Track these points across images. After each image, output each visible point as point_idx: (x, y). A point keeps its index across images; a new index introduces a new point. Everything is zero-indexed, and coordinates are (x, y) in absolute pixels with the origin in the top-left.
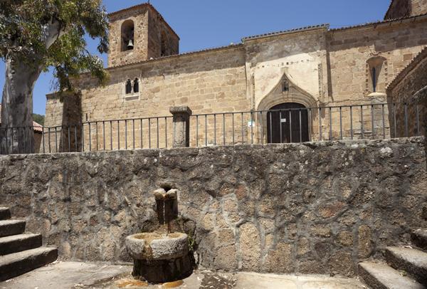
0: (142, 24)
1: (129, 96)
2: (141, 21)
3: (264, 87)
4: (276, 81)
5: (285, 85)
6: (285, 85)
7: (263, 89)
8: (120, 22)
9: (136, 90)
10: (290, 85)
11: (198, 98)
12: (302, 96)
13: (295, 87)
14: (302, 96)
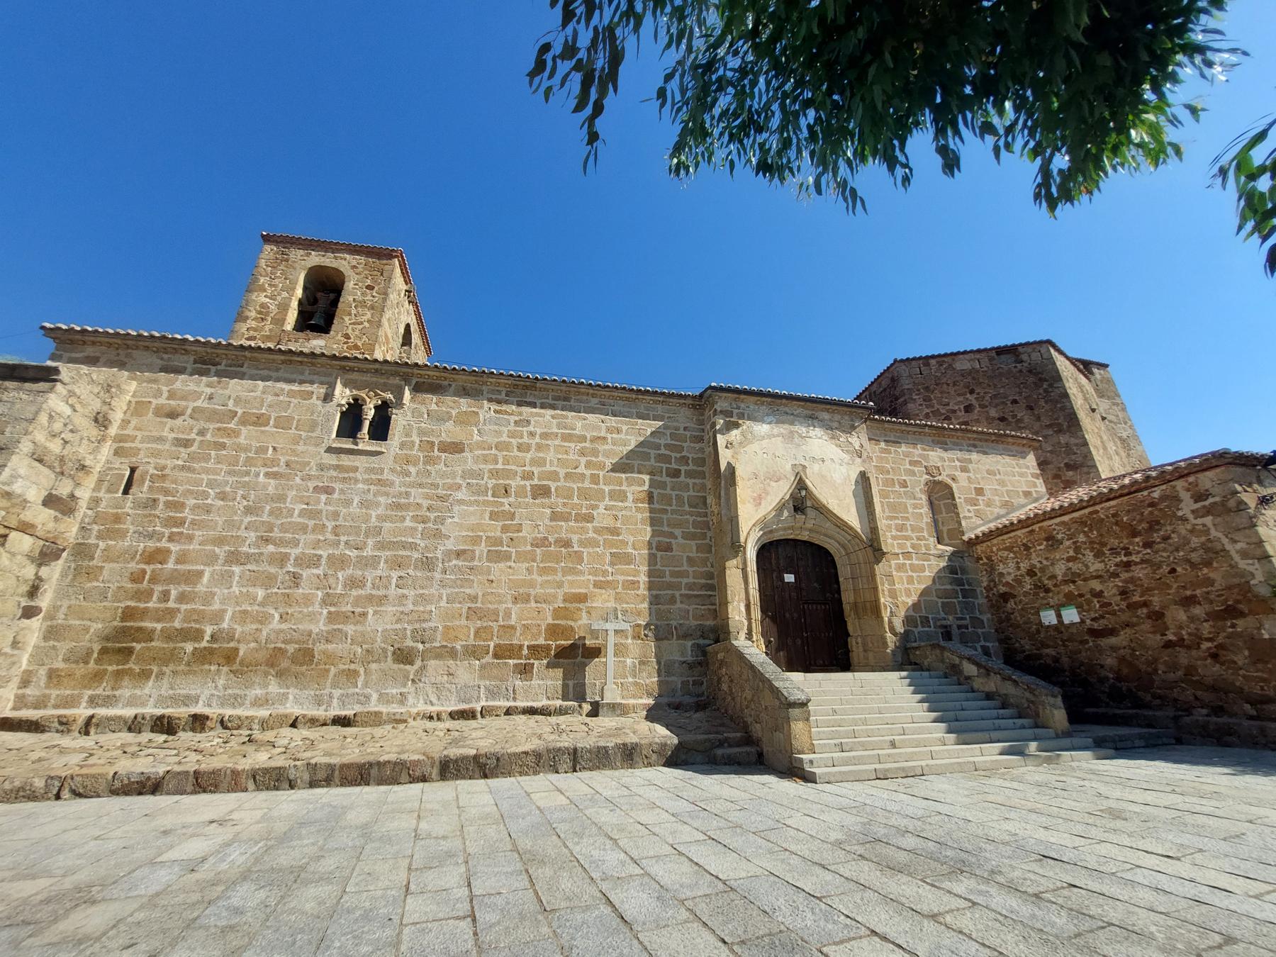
0: (370, 288)
1: (347, 444)
2: (369, 282)
3: (760, 497)
4: (782, 490)
5: (801, 500)
6: (801, 500)
7: (758, 501)
8: (304, 262)
9: (381, 430)
10: (809, 503)
11: (584, 494)
12: (832, 530)
13: (822, 510)
14: (832, 530)
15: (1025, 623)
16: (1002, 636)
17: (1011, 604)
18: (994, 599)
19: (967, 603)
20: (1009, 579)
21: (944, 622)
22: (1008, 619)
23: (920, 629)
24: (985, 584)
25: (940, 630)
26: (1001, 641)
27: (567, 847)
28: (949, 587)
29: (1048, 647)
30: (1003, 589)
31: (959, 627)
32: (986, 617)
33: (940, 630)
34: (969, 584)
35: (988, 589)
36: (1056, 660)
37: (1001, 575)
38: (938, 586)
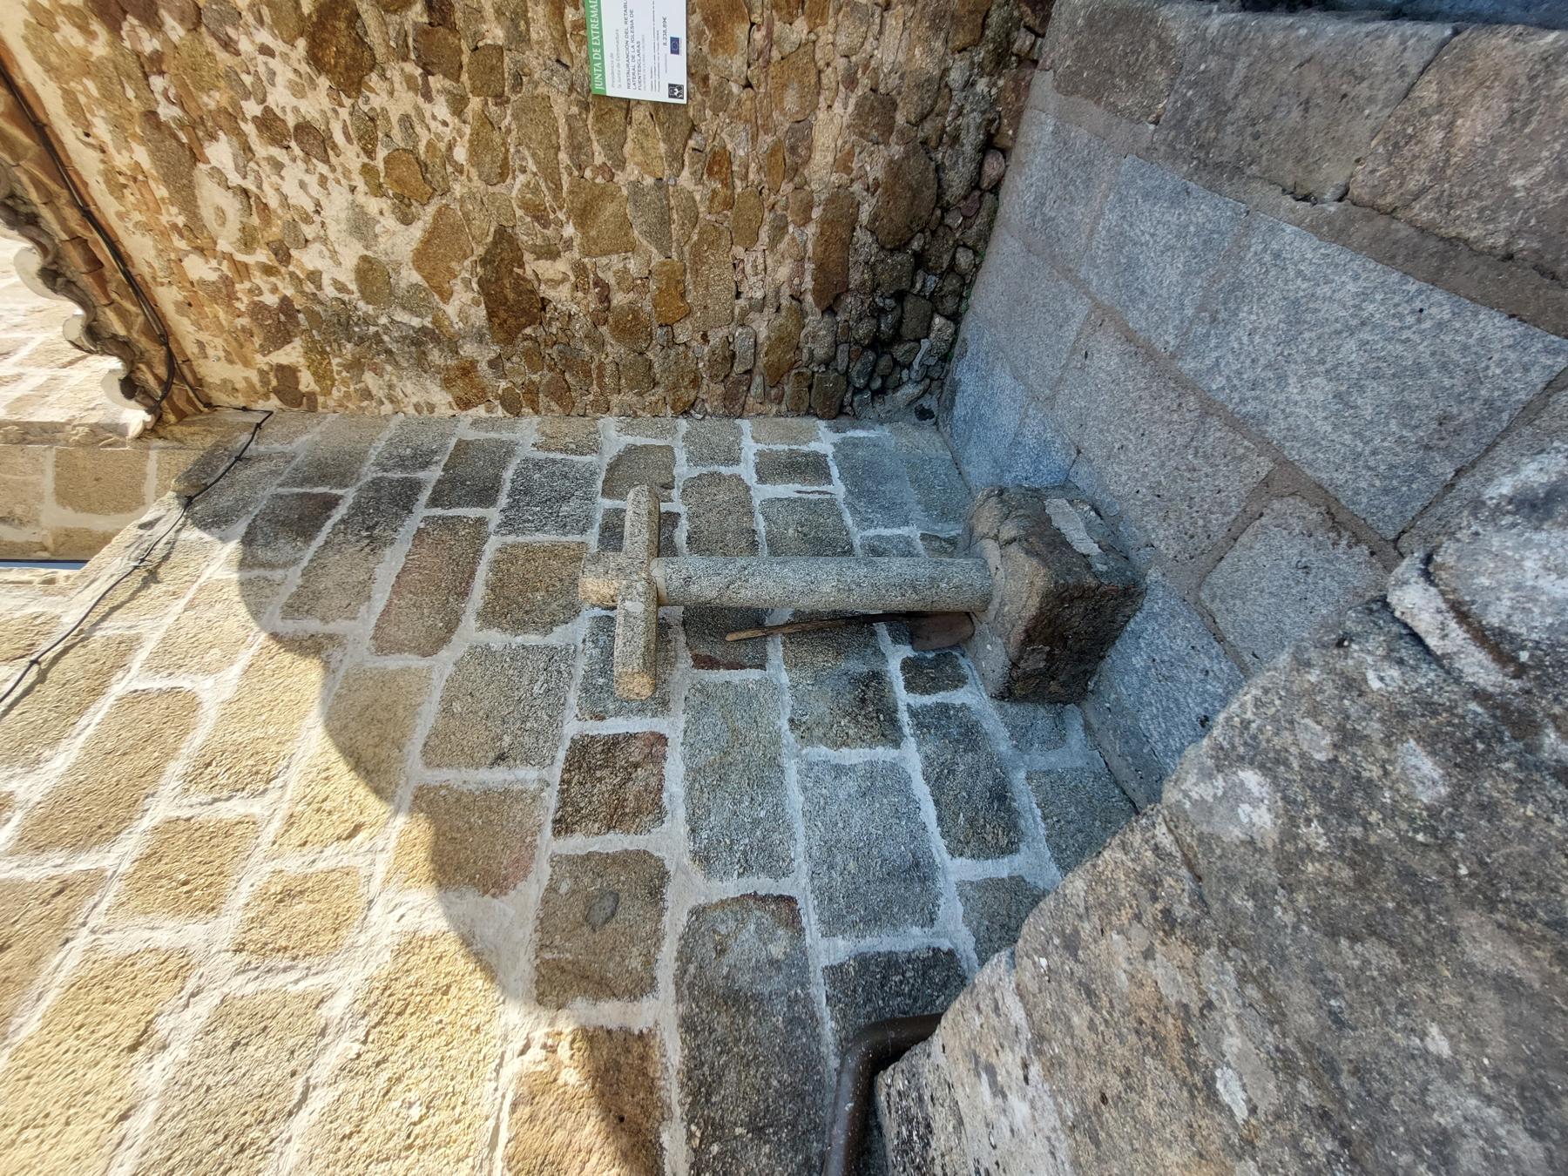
15: (660, 231)
16: (712, 391)
17: (550, 276)
18: (520, 373)
19: (523, 491)
20: (400, 241)
21: (630, 643)
22: (631, 328)
23: (669, 840)
24: (441, 399)
25: (684, 674)
26: (733, 406)
27: (839, 1081)
28: (391, 562)
29: (802, 131)
30: (462, 306)
31: (663, 547)
32: (614, 435)
33: (684, 674)
34: (423, 459)
35: (465, 384)
36: (877, 112)
37: (370, 274)
38: (361, 627)
